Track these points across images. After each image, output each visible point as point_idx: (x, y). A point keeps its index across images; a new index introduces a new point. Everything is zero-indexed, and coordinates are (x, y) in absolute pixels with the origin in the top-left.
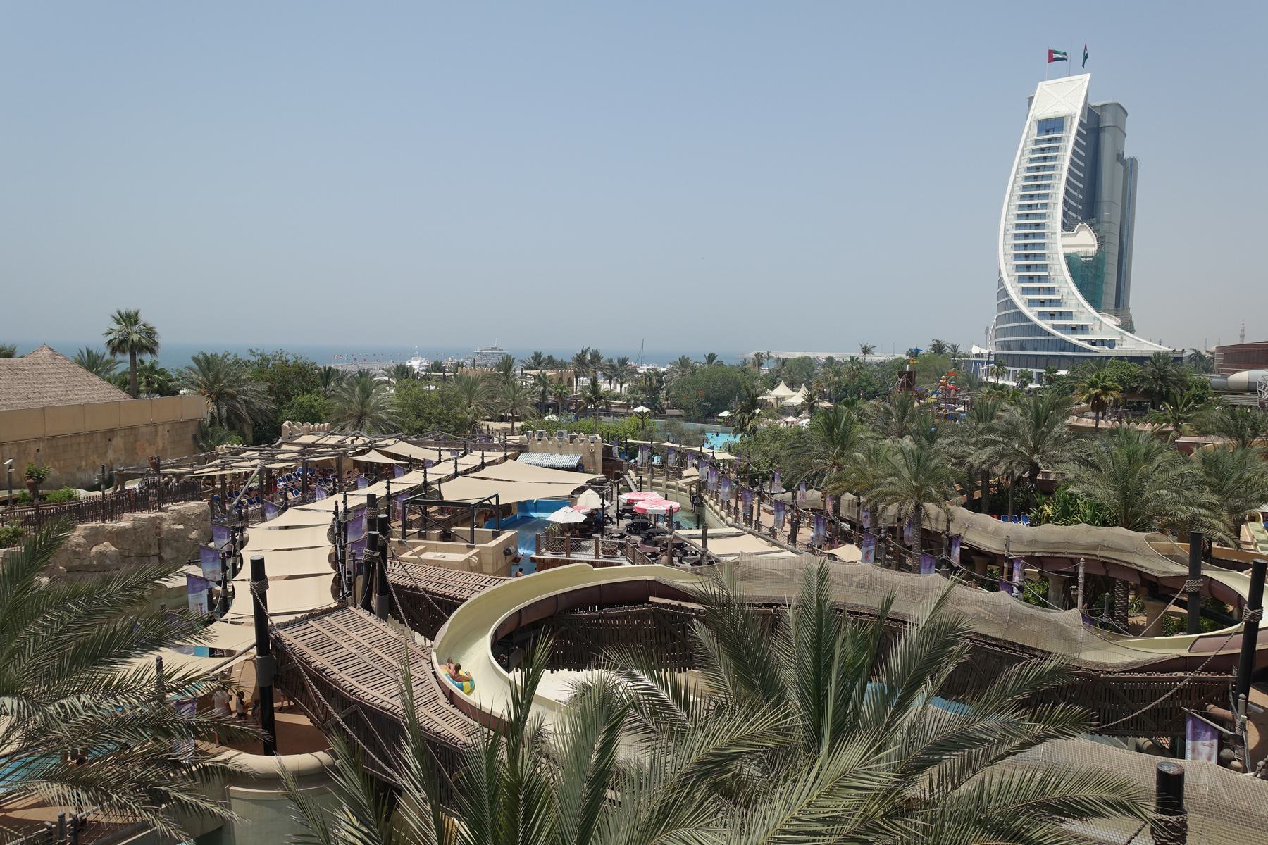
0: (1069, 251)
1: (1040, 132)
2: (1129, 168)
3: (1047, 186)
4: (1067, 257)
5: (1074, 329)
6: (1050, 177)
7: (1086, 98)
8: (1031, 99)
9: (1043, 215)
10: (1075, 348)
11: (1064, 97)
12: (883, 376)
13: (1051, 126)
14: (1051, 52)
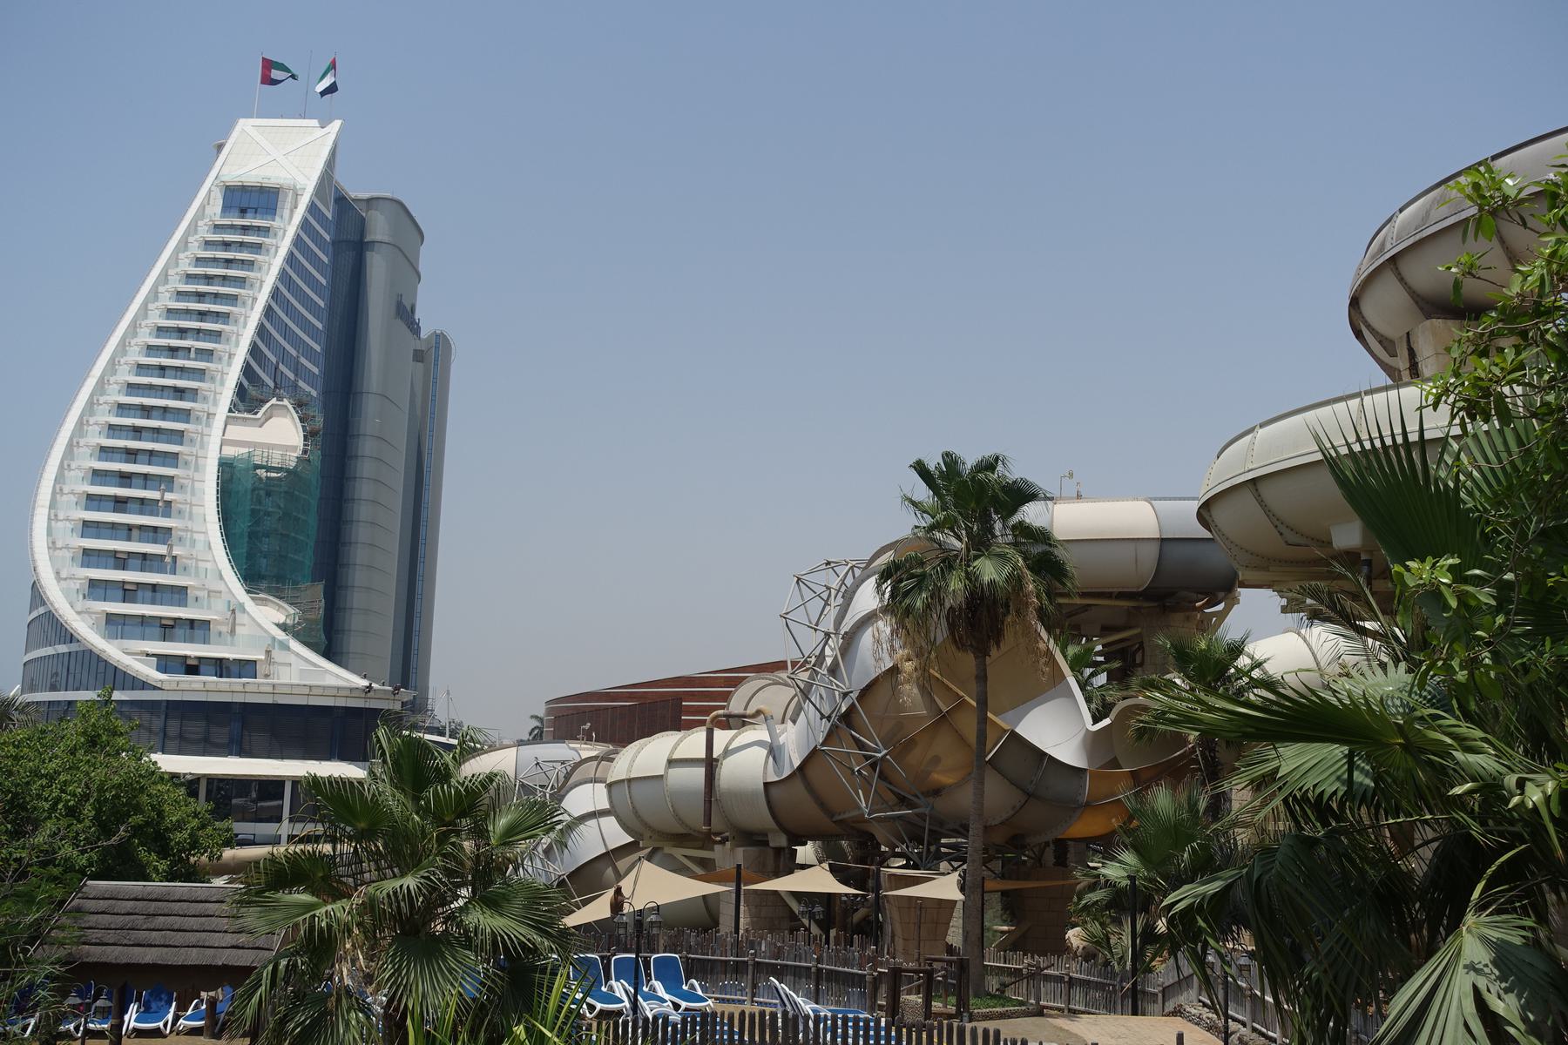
0: (230, 451)
1: (226, 208)
2: (433, 357)
3: (223, 317)
4: (226, 466)
6: (233, 299)
7: (330, 164)
8: (220, 147)
9: (200, 374)
10: (118, 677)
11: (286, 152)
13: (253, 202)
14: (268, 65)
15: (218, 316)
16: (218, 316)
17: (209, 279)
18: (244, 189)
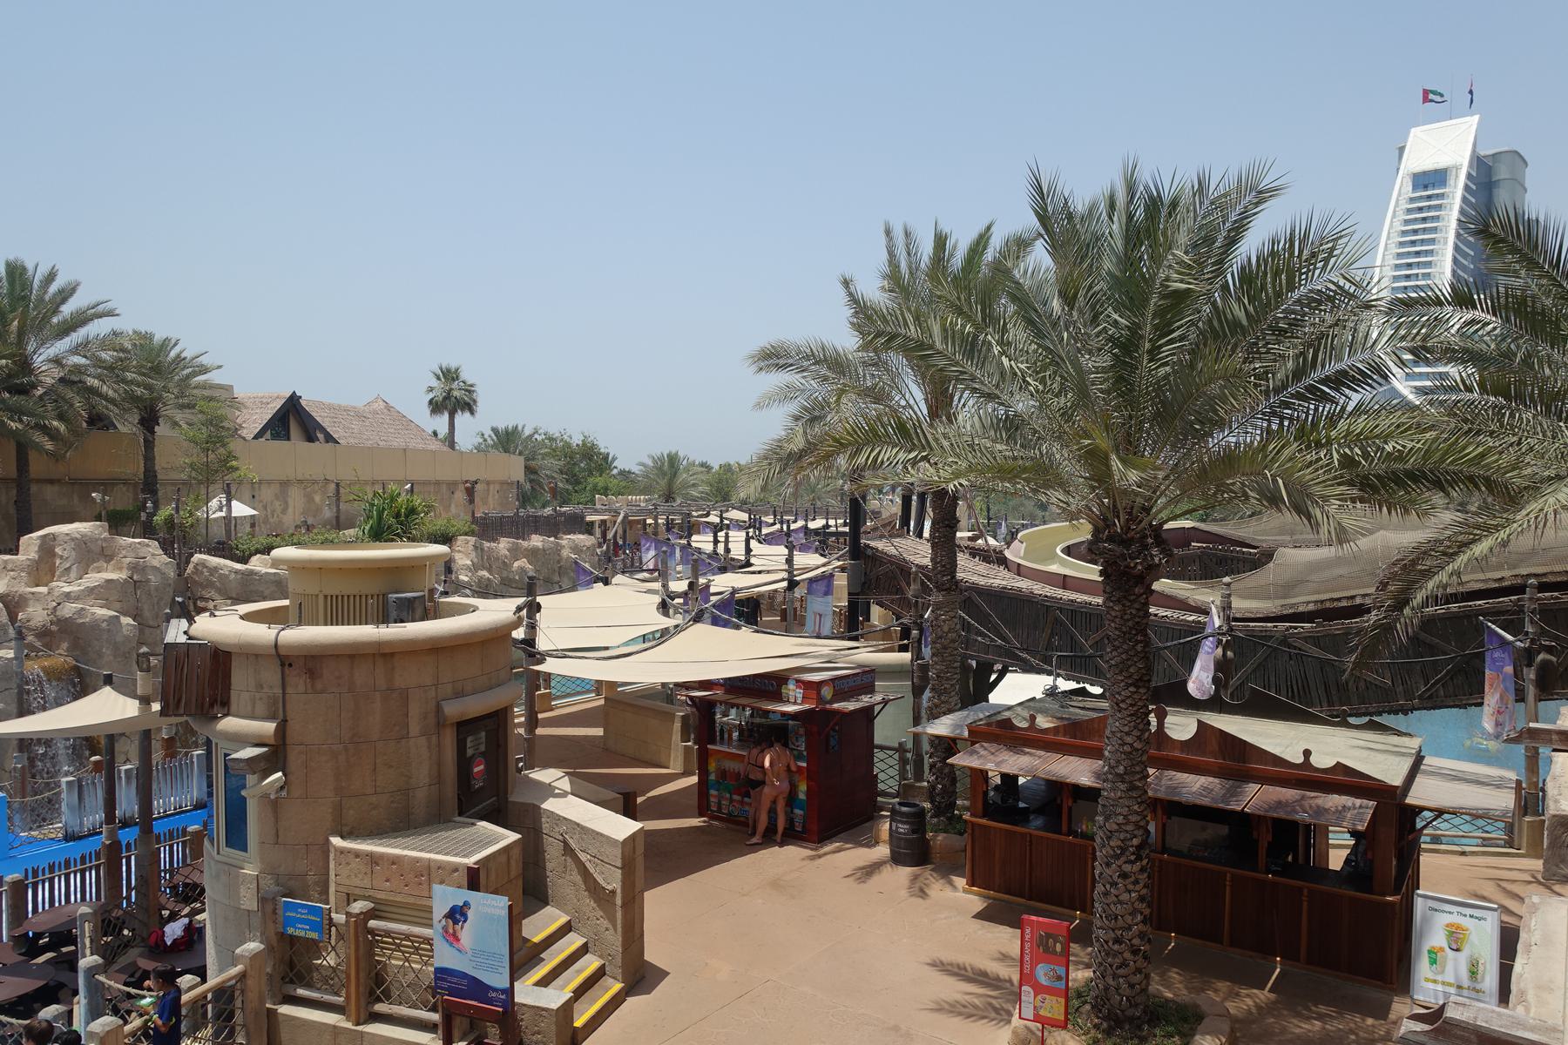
7: (1475, 145)
8: (1402, 150)
11: (1446, 144)
14: (1426, 93)
15: (1427, 253)
16: (1427, 253)
17: (1415, 232)
18: (1425, 173)
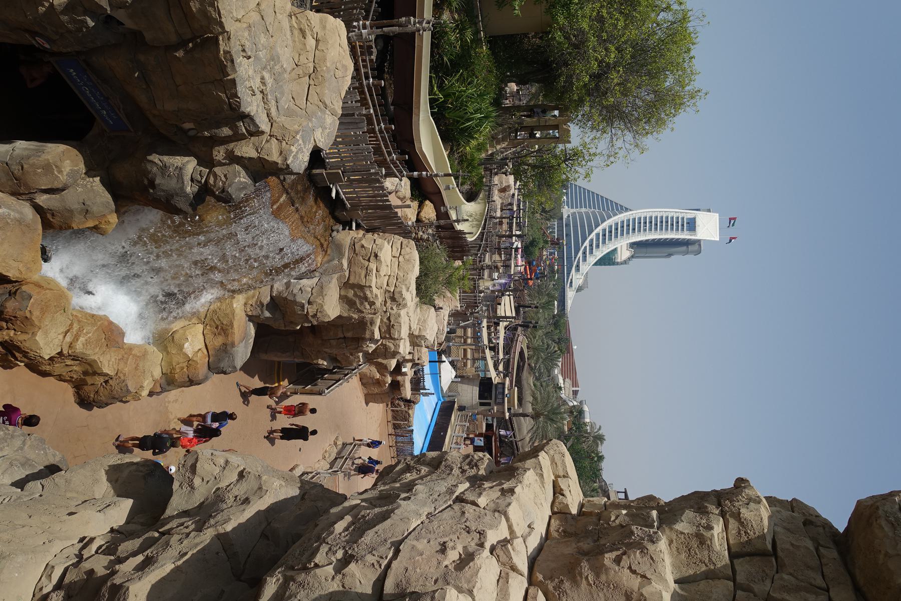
0: (619, 250)
2: (670, 255)
4: (616, 250)
5: (584, 253)
8: (709, 211)
11: (708, 228)
12: (684, 70)
13: (691, 225)
14: (735, 219)
